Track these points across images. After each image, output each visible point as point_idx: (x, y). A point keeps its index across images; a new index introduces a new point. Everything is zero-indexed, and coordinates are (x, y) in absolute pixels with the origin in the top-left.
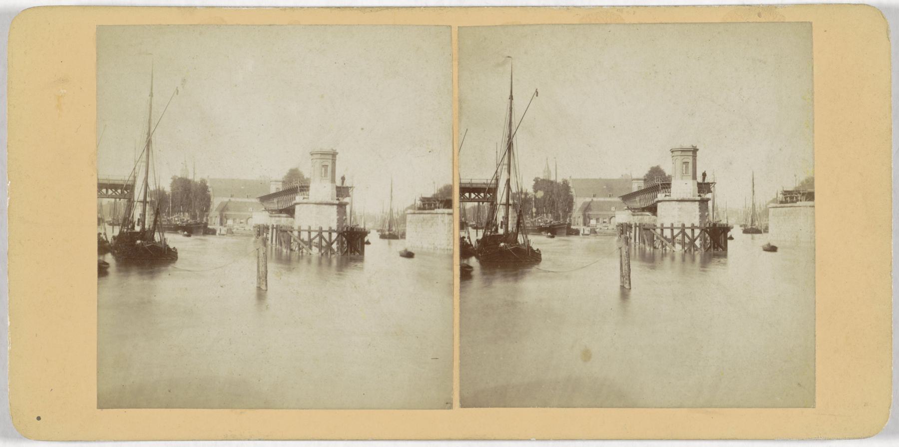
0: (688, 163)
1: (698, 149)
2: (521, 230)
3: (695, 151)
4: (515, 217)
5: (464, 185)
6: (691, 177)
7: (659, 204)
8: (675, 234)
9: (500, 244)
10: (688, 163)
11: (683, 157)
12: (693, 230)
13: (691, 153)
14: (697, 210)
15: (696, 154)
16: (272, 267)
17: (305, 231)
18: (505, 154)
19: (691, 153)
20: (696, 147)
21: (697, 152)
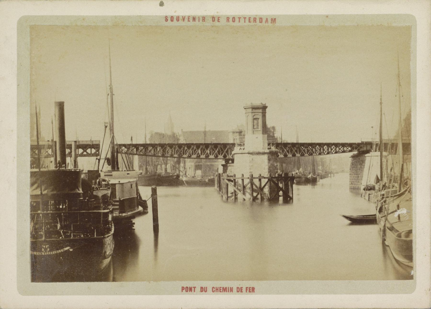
0: (259, 119)
1: (267, 106)
2: (254, 191)
3: (264, 108)
4: (99, 191)
5: (82, 142)
6: (261, 132)
7: (235, 155)
8: (263, 185)
9: (73, 250)
10: (259, 119)
11: (254, 114)
12: (260, 180)
13: (261, 111)
14: (266, 161)
15: (265, 111)
16: (218, 158)
17: (257, 178)
18: (110, 145)
19: (261, 111)
20: (265, 104)
21: (267, 109)
